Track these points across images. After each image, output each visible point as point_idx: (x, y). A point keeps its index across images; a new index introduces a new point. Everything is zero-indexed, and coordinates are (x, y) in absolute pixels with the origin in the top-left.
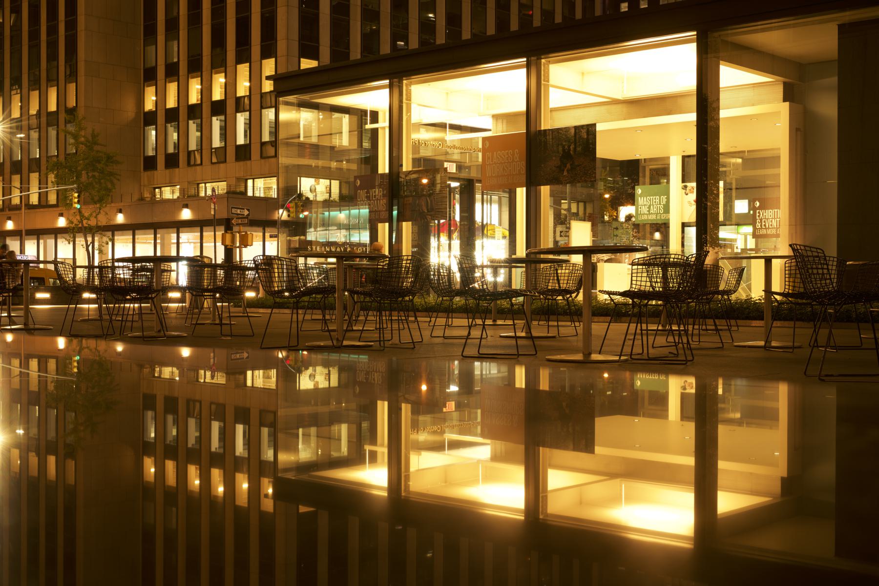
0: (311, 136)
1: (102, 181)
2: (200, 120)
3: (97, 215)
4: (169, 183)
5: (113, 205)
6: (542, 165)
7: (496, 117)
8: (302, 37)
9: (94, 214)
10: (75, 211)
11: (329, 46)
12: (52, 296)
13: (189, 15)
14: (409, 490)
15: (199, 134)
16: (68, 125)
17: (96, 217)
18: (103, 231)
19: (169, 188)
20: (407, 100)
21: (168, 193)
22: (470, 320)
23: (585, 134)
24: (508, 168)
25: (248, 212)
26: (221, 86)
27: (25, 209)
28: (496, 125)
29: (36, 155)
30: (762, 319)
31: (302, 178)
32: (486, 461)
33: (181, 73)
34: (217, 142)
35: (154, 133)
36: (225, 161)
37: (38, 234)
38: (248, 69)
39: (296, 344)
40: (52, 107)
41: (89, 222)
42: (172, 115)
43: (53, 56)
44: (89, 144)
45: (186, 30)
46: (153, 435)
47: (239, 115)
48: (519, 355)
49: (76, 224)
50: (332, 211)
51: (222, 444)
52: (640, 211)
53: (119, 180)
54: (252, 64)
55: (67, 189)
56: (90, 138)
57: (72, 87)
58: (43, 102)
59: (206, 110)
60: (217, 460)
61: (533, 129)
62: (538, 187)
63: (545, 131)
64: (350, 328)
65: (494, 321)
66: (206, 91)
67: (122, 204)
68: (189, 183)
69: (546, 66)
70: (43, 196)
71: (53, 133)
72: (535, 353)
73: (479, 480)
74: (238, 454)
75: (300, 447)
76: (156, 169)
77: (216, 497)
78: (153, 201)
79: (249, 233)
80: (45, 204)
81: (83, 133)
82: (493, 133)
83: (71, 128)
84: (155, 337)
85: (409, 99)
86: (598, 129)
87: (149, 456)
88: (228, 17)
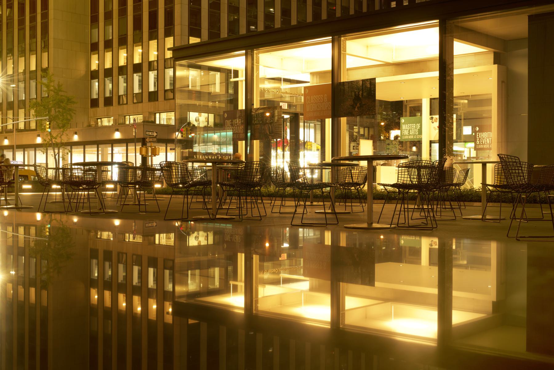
0: (196, 86)
1: (64, 114)
5: (71, 129)
7: (313, 74)
8: (190, 23)
9: (59, 135)
10: (47, 133)
11: (207, 29)
12: (33, 187)
13: (119, 10)
16: (43, 79)
17: (60, 137)
18: (65, 146)
20: (256, 63)
21: (106, 122)
22: (297, 202)
23: (369, 85)
25: (156, 134)
27: (16, 132)
29: (23, 98)
31: (190, 113)
34: (137, 90)
35: (97, 84)
37: (24, 147)
38: (157, 43)
39: (187, 217)
40: (33, 68)
41: (56, 140)
42: (108, 73)
43: (33, 36)
45: (117, 19)
46: (96, 275)
47: (150, 73)
48: (327, 224)
51: (140, 280)
53: (75, 114)
55: (42, 119)
56: (57, 87)
58: (27, 64)
59: (130, 69)
60: (137, 290)
61: (336, 81)
62: (339, 118)
63: (343, 82)
64: (220, 207)
65: (312, 202)
66: (130, 57)
67: (77, 129)
71: (33, 83)
74: (150, 286)
75: (189, 282)
76: (99, 107)
77: (136, 314)
78: (96, 127)
79: (157, 147)
81: (52, 84)
82: (311, 84)
83: (45, 81)
84: (98, 213)
85: (258, 62)
86: (377, 81)
87: (94, 288)
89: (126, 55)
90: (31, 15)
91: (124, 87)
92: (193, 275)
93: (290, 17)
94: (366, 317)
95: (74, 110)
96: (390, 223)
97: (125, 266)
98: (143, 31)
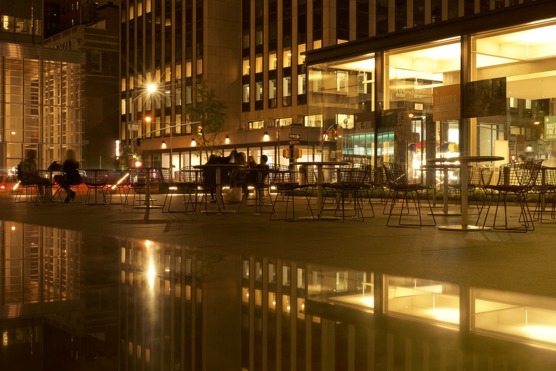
0: (344, 87)
1: (217, 118)
2: (276, 80)
3: (213, 139)
4: (258, 119)
5: (223, 133)
6: (471, 105)
7: (445, 74)
8: (339, 26)
9: (212, 139)
10: (200, 137)
11: (356, 31)
12: (178, 189)
13: (269, 15)
14: (388, 310)
15: (275, 88)
16: (198, 85)
17: (213, 141)
18: (217, 149)
19: (258, 122)
20: (386, 65)
21: (257, 125)
22: (417, 204)
23: (499, 84)
24: (449, 107)
25: (299, 137)
26: (289, 58)
27: (172, 136)
28: (446, 78)
29: (180, 104)
30: (317, 196)
31: (339, 115)
32: (439, 294)
33: (264, 51)
34: (286, 93)
35: (248, 88)
36: (291, 105)
37: (180, 151)
38: (305, 47)
39: (293, 218)
40: (189, 74)
41: (209, 144)
42: (259, 77)
43: (189, 45)
44: (209, 96)
45: (268, 25)
46: (248, 274)
47: (299, 76)
48: (421, 225)
49: (201, 145)
50: (361, 135)
51: (289, 281)
52: (548, 133)
53: (226, 118)
54: (308, 44)
55: (196, 123)
56: (210, 93)
57: (200, 62)
58: (184, 71)
59: (266, 76)
60: (286, 290)
61: (465, 81)
62: (469, 119)
63: (473, 82)
64: (338, 209)
65: (434, 204)
66: (280, 61)
67: (229, 132)
68: (269, 119)
69: (474, 40)
70: (183, 128)
71: (189, 90)
72: (435, 224)
73: (525, 320)
74: (299, 287)
75: (337, 283)
76: (250, 111)
77: (286, 313)
78: (248, 131)
79: (299, 149)
80: (184, 133)
81: (206, 90)
82: (444, 84)
83: (199, 87)
84: (216, 213)
85: (388, 64)
86: (507, 81)
87: (246, 287)
88: (293, 16)
89: (275, 59)
90: (187, 24)
91: (274, 91)
92: (342, 278)
93: (441, 16)
94: (499, 322)
95: (225, 115)
96: (493, 225)
97: (275, 266)
98: (293, 36)
